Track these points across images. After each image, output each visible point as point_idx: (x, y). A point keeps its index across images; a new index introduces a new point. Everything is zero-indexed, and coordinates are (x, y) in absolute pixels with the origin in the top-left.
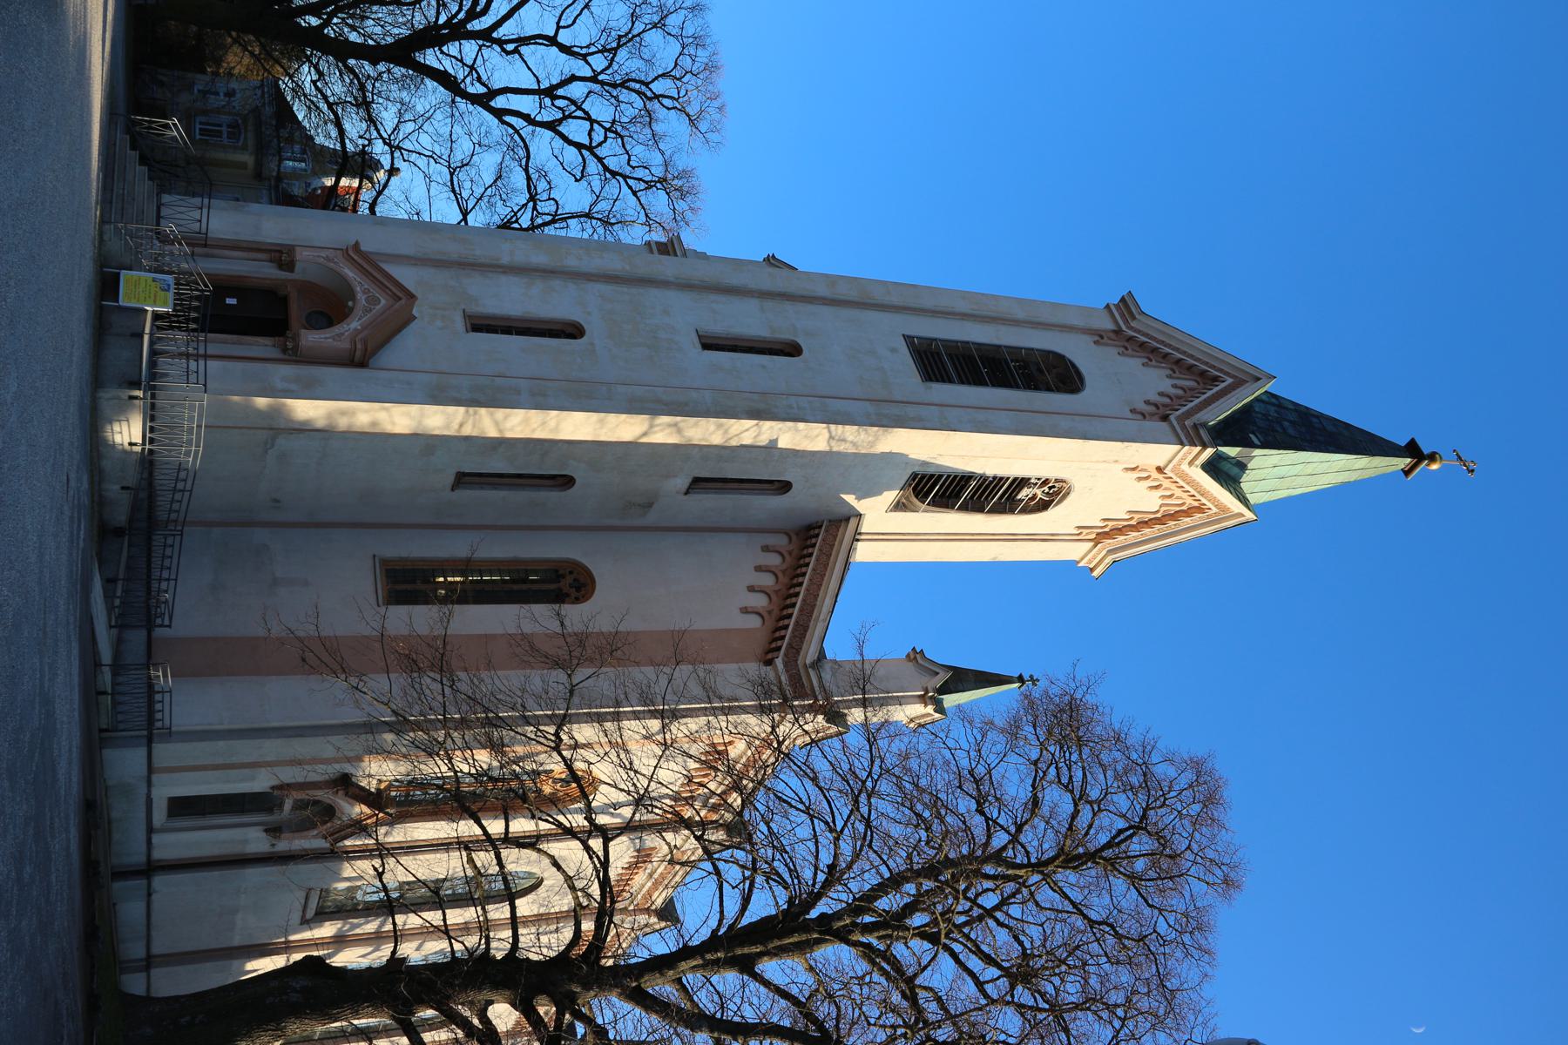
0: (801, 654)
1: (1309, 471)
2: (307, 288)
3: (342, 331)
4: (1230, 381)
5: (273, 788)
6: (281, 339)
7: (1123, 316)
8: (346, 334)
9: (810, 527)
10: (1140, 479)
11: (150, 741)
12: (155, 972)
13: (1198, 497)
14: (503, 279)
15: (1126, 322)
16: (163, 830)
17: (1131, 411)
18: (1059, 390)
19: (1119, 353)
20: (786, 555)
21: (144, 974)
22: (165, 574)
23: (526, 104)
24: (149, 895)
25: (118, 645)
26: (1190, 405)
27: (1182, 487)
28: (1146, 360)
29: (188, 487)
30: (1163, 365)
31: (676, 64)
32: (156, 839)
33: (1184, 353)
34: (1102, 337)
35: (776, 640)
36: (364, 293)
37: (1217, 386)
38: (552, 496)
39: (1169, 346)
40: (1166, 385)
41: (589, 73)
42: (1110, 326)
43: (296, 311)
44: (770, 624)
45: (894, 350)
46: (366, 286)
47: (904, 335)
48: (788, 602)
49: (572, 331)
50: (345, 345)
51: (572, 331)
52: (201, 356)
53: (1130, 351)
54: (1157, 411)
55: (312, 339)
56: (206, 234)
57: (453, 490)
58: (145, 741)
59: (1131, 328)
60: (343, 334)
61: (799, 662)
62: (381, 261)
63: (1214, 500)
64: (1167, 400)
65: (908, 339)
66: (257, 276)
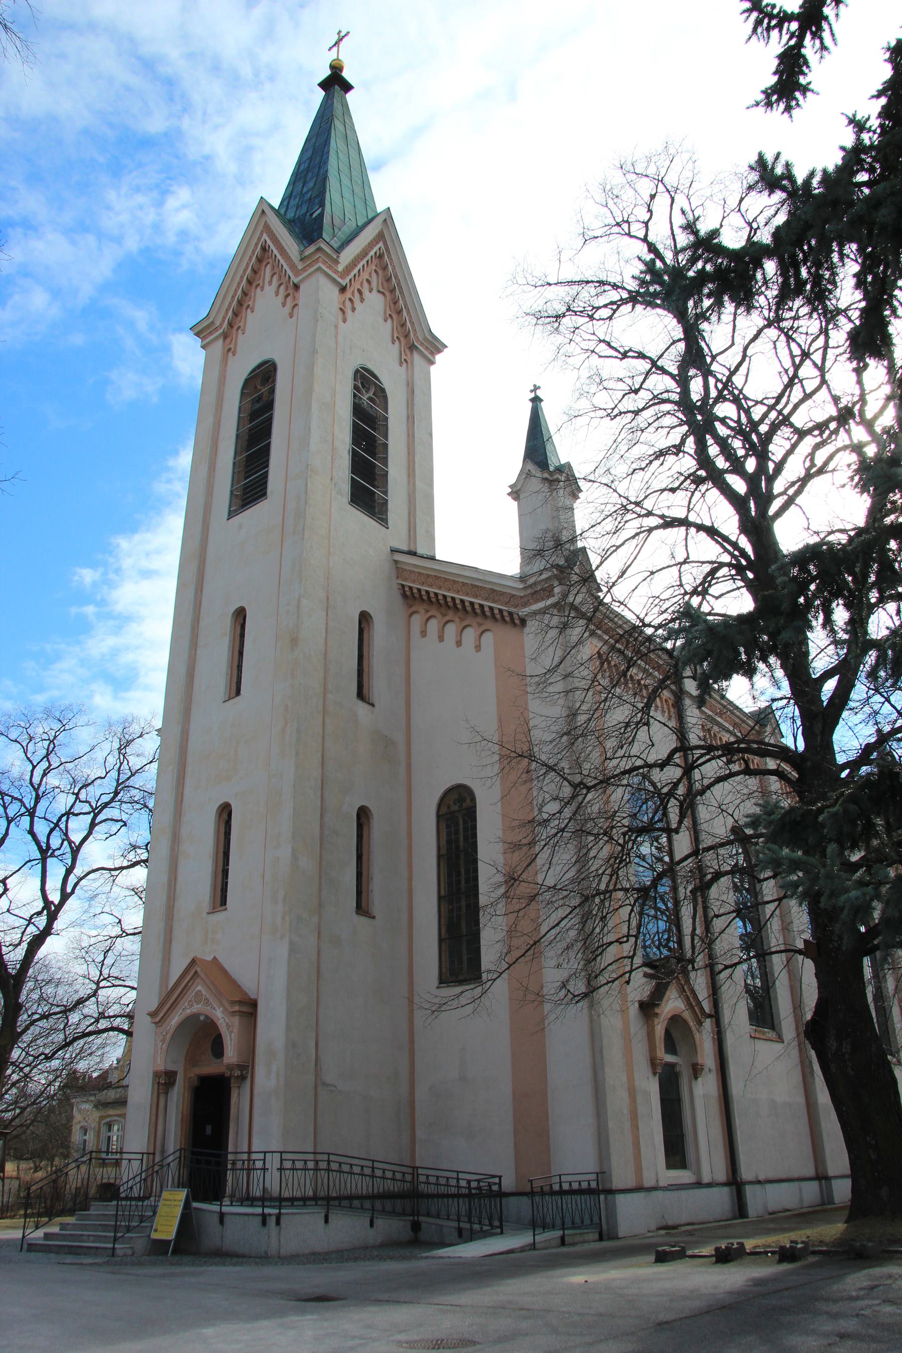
0: (514, 593)
2: (192, 1060)
3: (224, 1025)
4: (265, 237)
5: (655, 1074)
6: (232, 1081)
7: (211, 333)
9: (404, 595)
11: (611, 1192)
12: (831, 1172)
13: (369, 257)
14: (181, 879)
15: (216, 329)
16: (698, 1172)
21: (833, 1182)
22: (453, 1182)
23: (56, 870)
26: (285, 267)
27: (359, 271)
29: (369, 1164)
31: (16, 741)
32: (706, 1179)
34: (230, 349)
36: (192, 1006)
39: (236, 291)
40: (270, 290)
41: (27, 819)
42: (221, 341)
43: (210, 1068)
44: (489, 624)
48: (469, 609)
49: (225, 812)
50: (236, 1020)
51: (225, 812)
52: (249, 1156)
55: (231, 1054)
56: (143, 1154)
57: (374, 917)
58: (610, 1197)
59: (221, 324)
60: (227, 1024)
61: (522, 595)
63: (371, 245)
64: (282, 288)
65: (231, 515)
66: (181, 1107)
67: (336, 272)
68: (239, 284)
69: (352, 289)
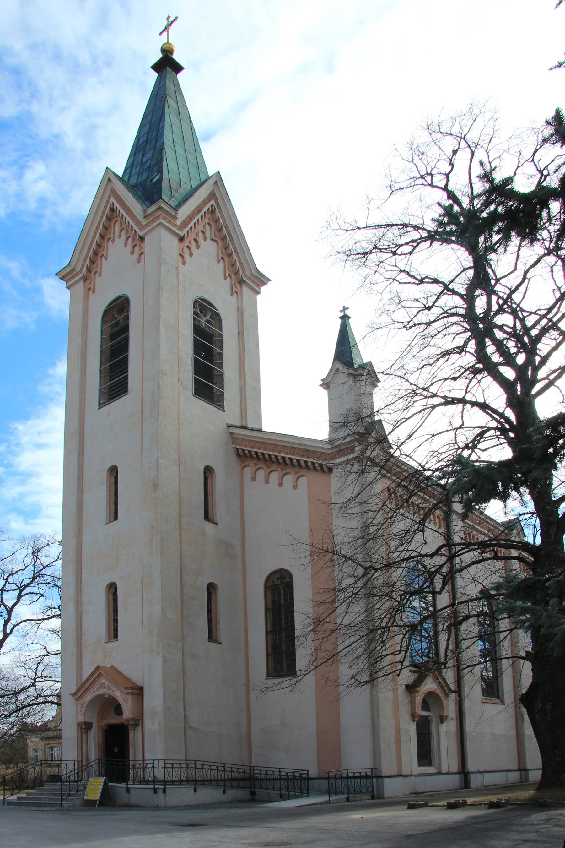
1: (181, 141)
4: (112, 200)
7: (73, 277)
8: (123, 697)
9: (238, 455)
10: (191, 255)
13: (202, 213)
14: (84, 625)
15: (77, 274)
17: (139, 262)
18: (128, 311)
19: (100, 276)
20: (257, 467)
24: (480, 772)
25: (320, 792)
26: (131, 223)
27: (195, 224)
28: (103, 258)
30: (105, 246)
33: (95, 233)
34: (90, 289)
35: (315, 467)
36: (99, 690)
37: (117, 207)
38: (222, 596)
39: (91, 244)
40: (119, 242)
42: (81, 284)
43: (114, 720)
45: (109, 413)
46: (95, 689)
47: (99, 409)
49: (113, 588)
51: (113, 588)
53: (98, 269)
54: (138, 245)
55: (128, 712)
59: (81, 270)
60: (124, 699)
61: (330, 452)
62: (81, 681)
63: (204, 203)
64: (130, 240)
65: (101, 406)
67: (175, 226)
68: (93, 238)
69: (189, 238)
